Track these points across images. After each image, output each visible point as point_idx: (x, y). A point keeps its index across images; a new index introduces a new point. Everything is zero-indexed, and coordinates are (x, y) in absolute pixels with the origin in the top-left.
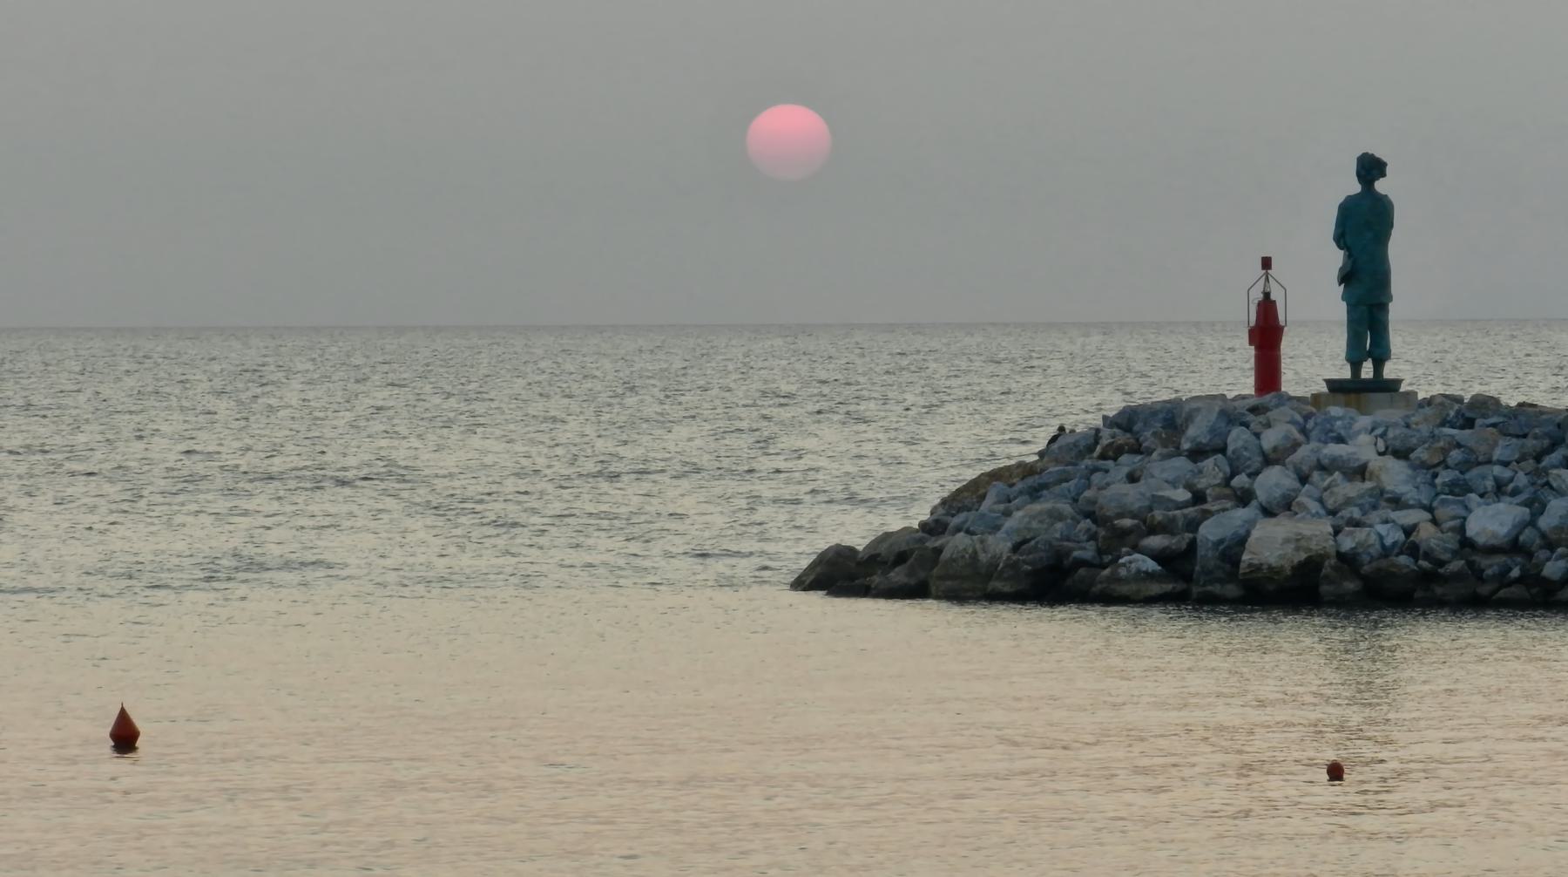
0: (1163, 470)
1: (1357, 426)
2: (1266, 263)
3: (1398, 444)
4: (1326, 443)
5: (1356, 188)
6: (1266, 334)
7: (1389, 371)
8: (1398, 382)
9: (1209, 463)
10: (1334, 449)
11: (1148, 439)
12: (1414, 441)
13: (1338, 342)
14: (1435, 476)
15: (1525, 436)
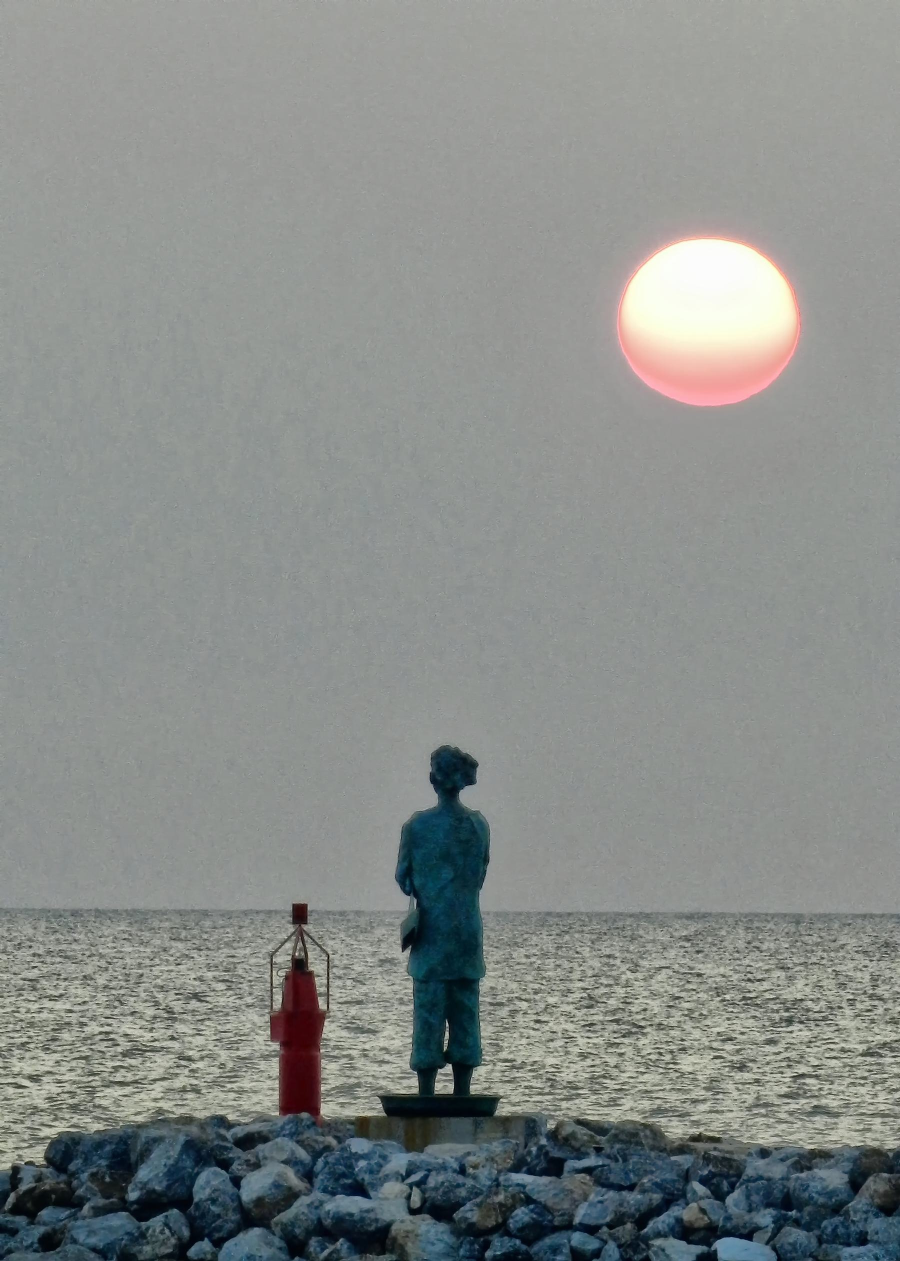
0: (91, 1233)
1: (389, 1168)
2: (300, 914)
3: (438, 1196)
4: (333, 1194)
5: (428, 799)
6: (299, 1026)
7: (481, 1082)
8: (493, 1101)
9: (156, 1223)
10: (349, 1205)
11: (84, 1185)
12: (463, 1192)
13: (397, 1037)
14: (486, 1246)
15: (631, 1188)
